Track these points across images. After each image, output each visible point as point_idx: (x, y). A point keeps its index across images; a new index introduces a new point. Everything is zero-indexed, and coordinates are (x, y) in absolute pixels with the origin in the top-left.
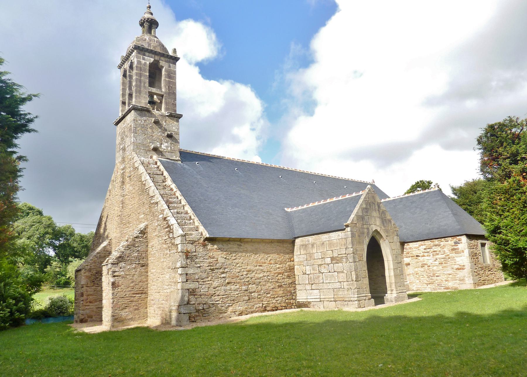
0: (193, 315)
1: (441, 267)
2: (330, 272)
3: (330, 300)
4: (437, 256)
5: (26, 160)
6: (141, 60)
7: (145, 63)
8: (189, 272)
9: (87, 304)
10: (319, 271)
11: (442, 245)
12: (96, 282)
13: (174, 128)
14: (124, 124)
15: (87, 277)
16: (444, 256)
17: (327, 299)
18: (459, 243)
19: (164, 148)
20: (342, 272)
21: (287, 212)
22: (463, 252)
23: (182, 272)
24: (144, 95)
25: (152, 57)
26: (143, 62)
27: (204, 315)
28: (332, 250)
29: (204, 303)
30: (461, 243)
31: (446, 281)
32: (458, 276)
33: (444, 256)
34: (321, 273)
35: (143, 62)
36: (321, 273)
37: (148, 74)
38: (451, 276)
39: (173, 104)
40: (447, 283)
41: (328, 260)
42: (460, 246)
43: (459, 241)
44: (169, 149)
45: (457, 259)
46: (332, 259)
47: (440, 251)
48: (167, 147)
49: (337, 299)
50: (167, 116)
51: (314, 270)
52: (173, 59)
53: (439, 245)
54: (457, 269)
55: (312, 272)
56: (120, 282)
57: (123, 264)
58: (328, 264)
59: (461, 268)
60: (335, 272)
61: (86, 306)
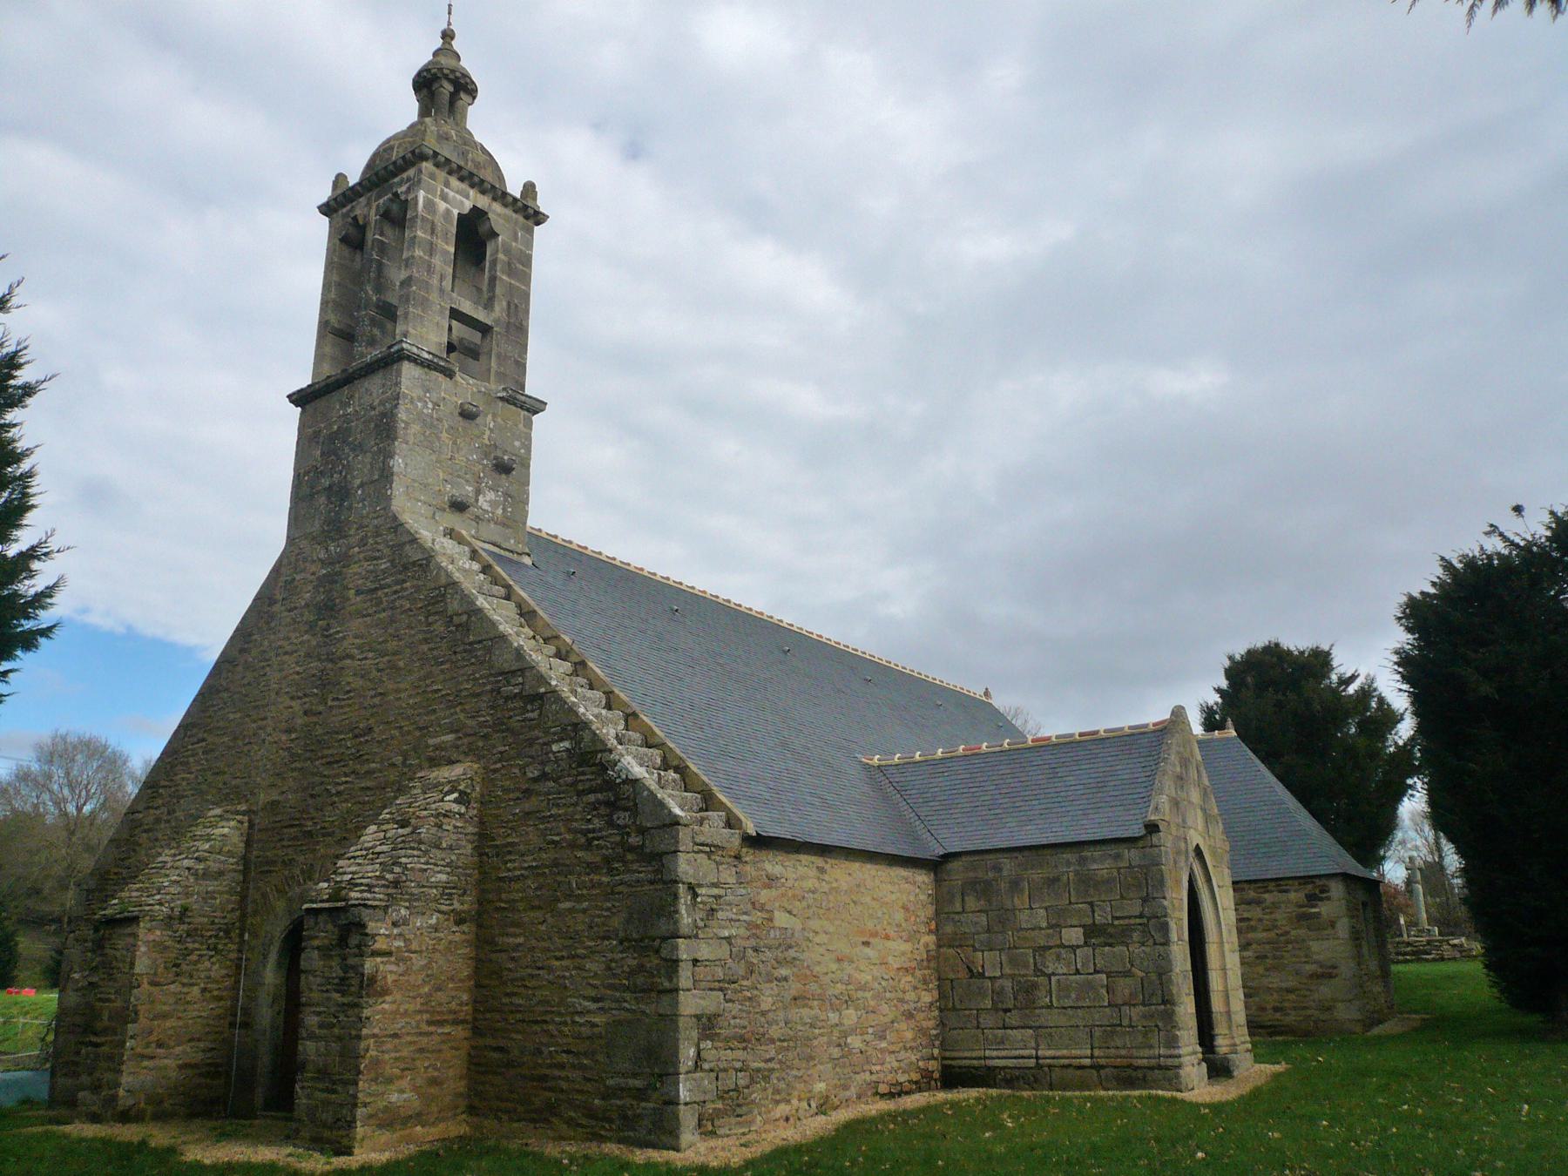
0: (710, 1107)
1: (1261, 970)
2: (1078, 972)
3: (1076, 1062)
4: (1251, 935)
5: (1443, 559)
6: (437, 200)
7: (448, 211)
8: (699, 956)
9: (148, 1051)
10: (1036, 969)
11: (1268, 903)
12: (184, 967)
13: (517, 444)
14: (345, 405)
15: (160, 947)
16: (1272, 935)
17: (1066, 1062)
18: (1321, 899)
19: (486, 506)
20: (1127, 974)
21: (1398, 792)
22: (1333, 924)
23: (676, 948)
24: (438, 318)
25: (467, 197)
26: (442, 206)
27: (739, 1111)
28: (1091, 904)
29: (738, 1065)
30: (1328, 899)
31: (1276, 1009)
32: (1316, 996)
33: (1272, 935)
34: (1044, 974)
35: (442, 206)
36: (1044, 974)
37: (452, 250)
38: (1292, 997)
39: (517, 362)
40: (1278, 1015)
41: (1074, 935)
42: (1324, 909)
43: (1322, 891)
44: (500, 511)
45: (1315, 946)
46: (1091, 931)
47: (1260, 920)
48: (493, 503)
49: (1102, 1062)
50: (502, 399)
51: (1013, 962)
52: (527, 217)
53: (1259, 902)
54: (1311, 976)
55: (1007, 971)
56: (390, 978)
57: (403, 912)
58: (1074, 948)
59: (1327, 973)
60: (1096, 972)
61: (143, 1057)
